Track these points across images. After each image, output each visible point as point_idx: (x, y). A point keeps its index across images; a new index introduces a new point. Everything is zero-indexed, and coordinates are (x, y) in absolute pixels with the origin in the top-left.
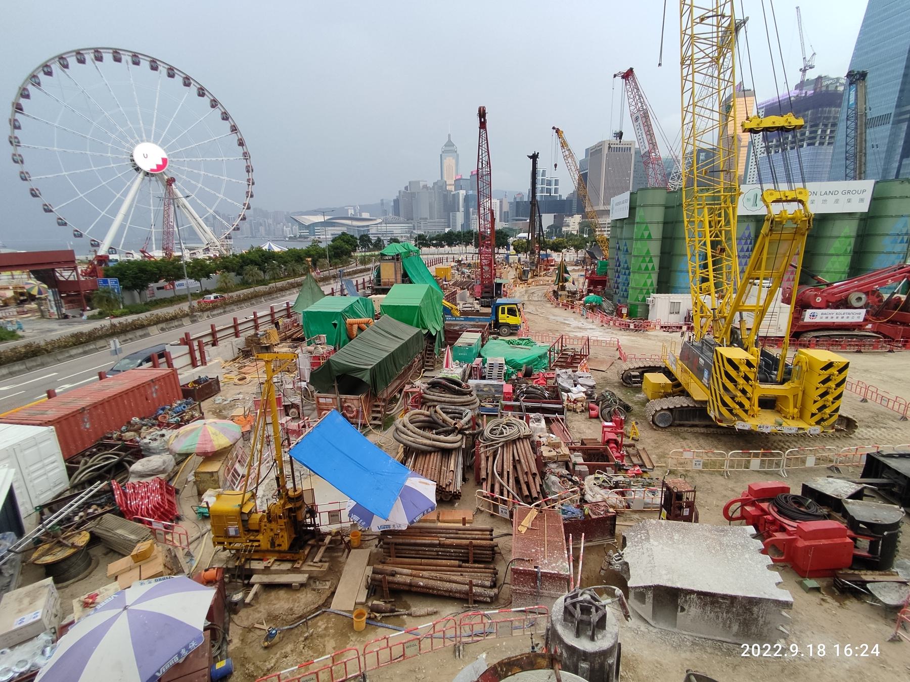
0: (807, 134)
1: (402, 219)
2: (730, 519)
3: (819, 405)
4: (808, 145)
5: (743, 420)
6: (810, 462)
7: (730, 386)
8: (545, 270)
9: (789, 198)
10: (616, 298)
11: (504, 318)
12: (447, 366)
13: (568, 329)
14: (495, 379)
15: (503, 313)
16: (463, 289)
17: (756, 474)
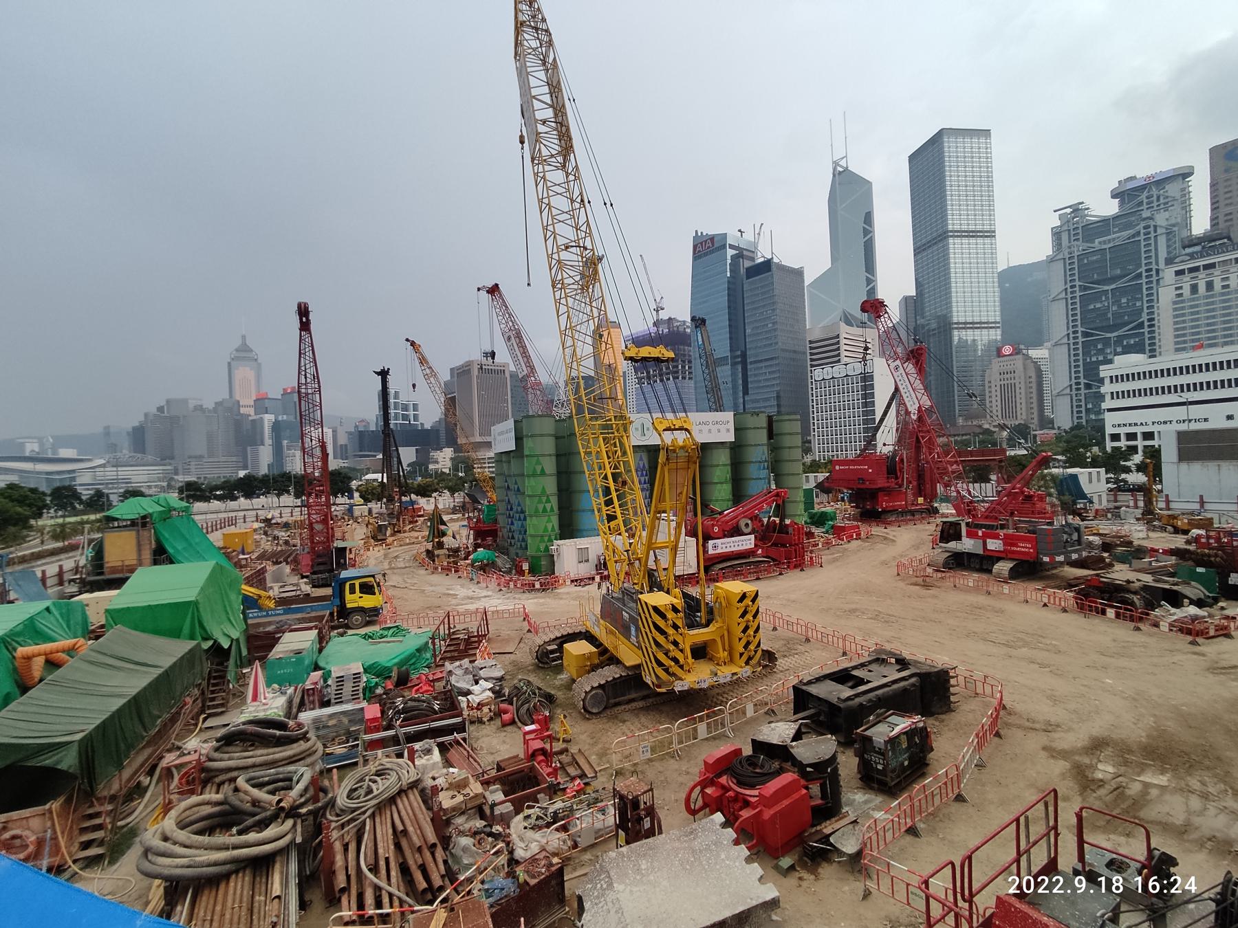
1: (150, 458)
3: (743, 642)
7: (661, 639)
8: (411, 522)
10: (512, 550)
11: (354, 600)
12: (255, 698)
13: (454, 602)
15: (352, 591)
16: (277, 563)
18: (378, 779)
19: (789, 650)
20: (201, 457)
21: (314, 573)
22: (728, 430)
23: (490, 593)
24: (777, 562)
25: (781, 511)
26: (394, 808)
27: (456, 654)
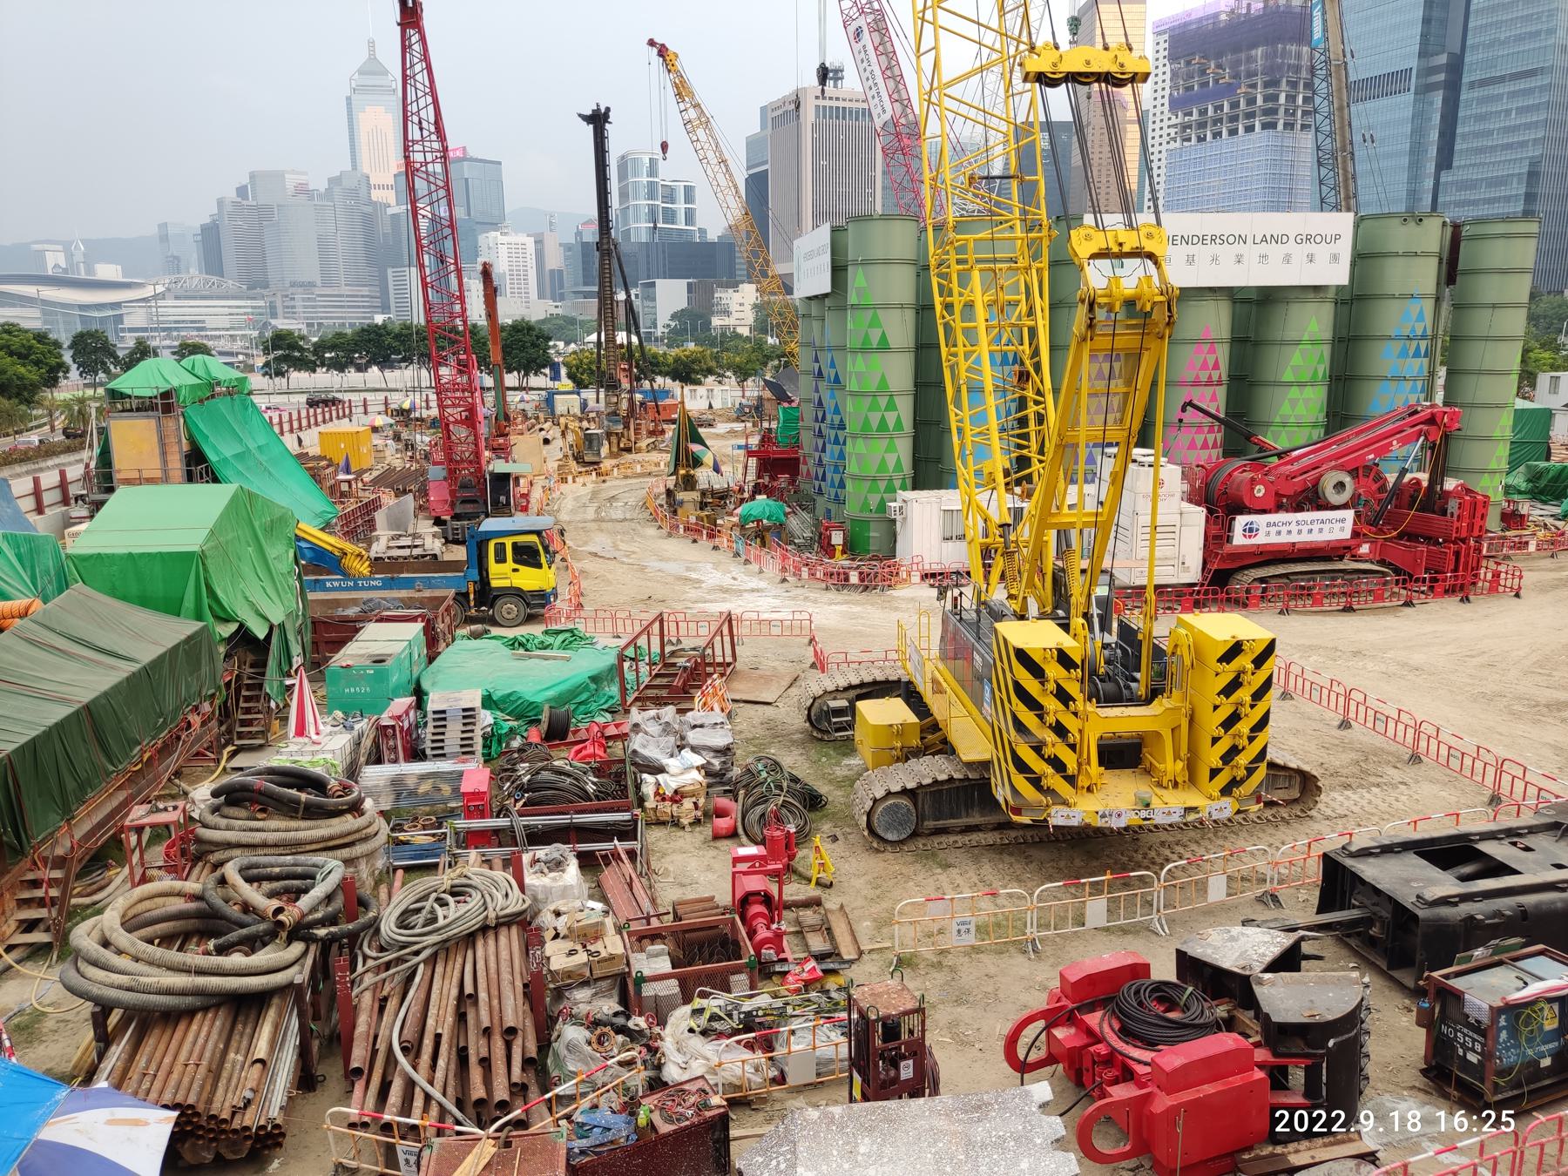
0: (1260, 101)
1: (230, 284)
2: (1023, 1068)
3: (1223, 746)
4: (1265, 126)
5: (1065, 803)
6: (1217, 890)
7: (1028, 718)
8: (651, 433)
9: (1126, 249)
10: (821, 503)
11: (503, 574)
12: (301, 731)
13: (693, 594)
14: (454, 756)
15: (501, 559)
16: (400, 493)
17: (1097, 933)
18: (451, 900)
19: (1362, 774)
20: (312, 285)
21: (456, 517)
22: (1335, 258)
23: (762, 584)
24: (1405, 577)
25: (1440, 461)
26: (470, 953)
27: (664, 693)
